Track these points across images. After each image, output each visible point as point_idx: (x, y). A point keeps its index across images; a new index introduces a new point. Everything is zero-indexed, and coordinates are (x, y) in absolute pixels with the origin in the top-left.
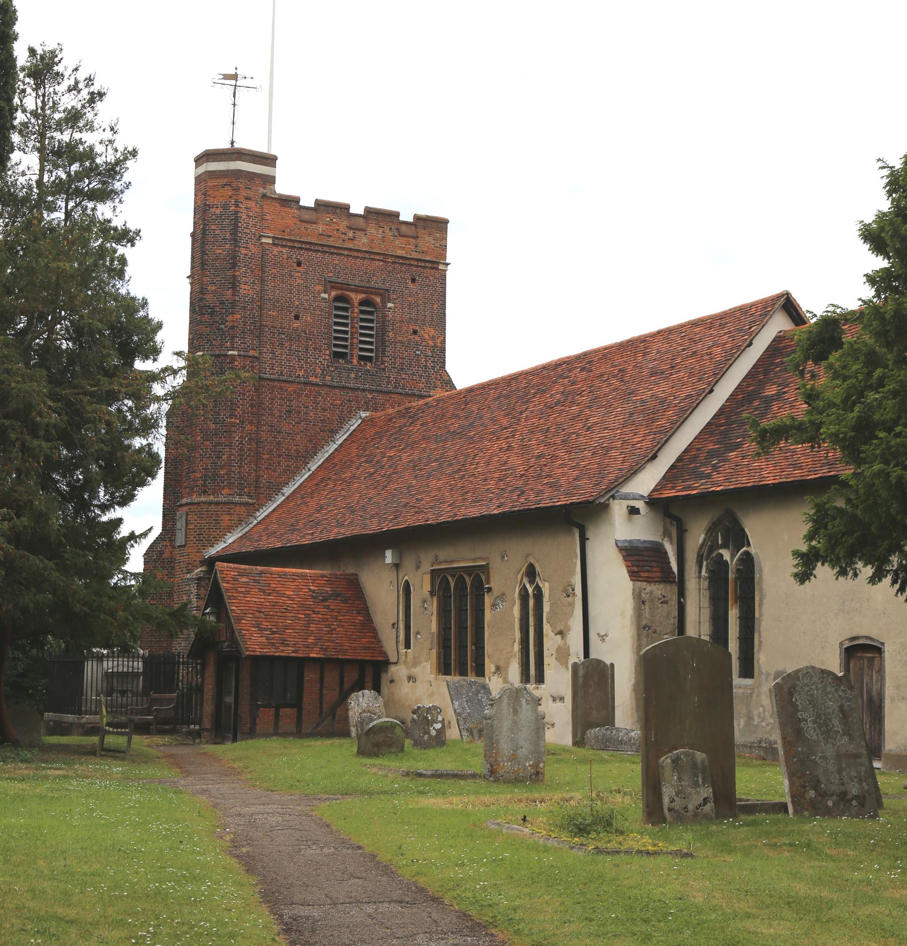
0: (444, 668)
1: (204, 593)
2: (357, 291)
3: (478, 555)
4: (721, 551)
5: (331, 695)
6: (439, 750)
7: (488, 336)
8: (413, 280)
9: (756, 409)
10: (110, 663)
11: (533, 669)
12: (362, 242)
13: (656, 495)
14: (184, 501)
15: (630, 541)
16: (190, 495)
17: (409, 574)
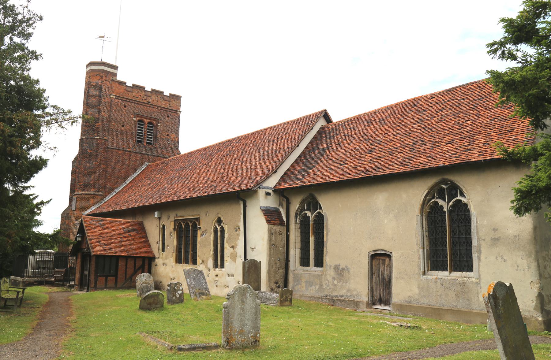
0: (179, 260)
2: (147, 119)
3: (195, 213)
4: (306, 212)
5: (130, 271)
6: (180, 305)
8: (168, 117)
9: (319, 153)
10: (38, 256)
11: (219, 261)
13: (277, 188)
14: (76, 193)
15: (266, 207)
16: (78, 191)
17: (165, 221)
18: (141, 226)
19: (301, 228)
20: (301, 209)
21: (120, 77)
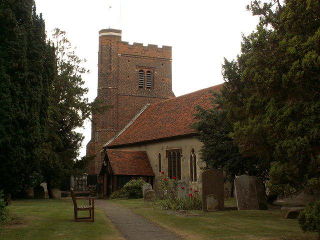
1: (103, 157)
2: (146, 68)
12: (147, 54)
21: (123, 39)
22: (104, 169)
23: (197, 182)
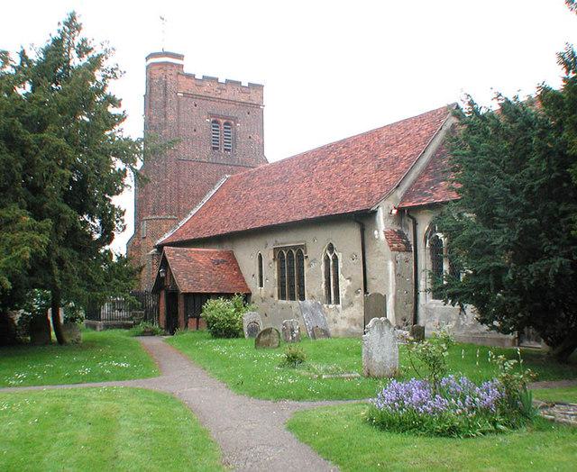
7: (286, 136)
12: (225, 95)
18: (231, 255)
19: (432, 253)
20: (432, 229)
22: (160, 284)
23: (339, 306)
